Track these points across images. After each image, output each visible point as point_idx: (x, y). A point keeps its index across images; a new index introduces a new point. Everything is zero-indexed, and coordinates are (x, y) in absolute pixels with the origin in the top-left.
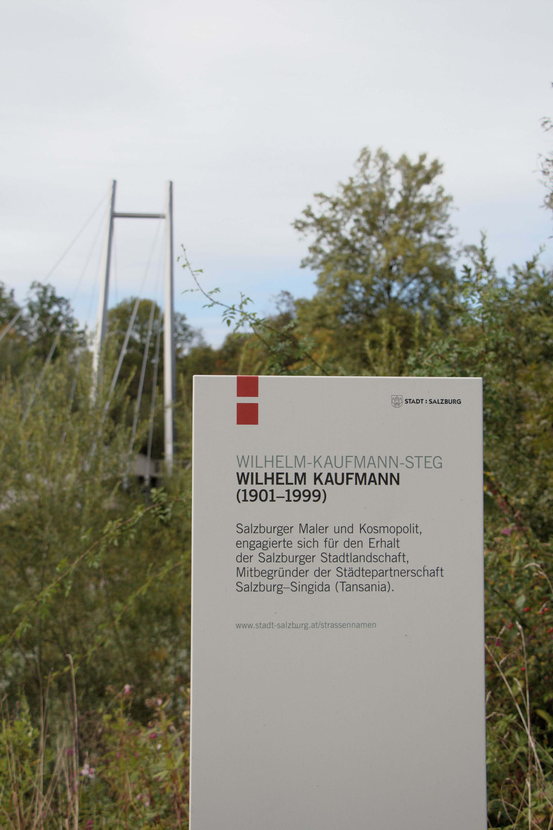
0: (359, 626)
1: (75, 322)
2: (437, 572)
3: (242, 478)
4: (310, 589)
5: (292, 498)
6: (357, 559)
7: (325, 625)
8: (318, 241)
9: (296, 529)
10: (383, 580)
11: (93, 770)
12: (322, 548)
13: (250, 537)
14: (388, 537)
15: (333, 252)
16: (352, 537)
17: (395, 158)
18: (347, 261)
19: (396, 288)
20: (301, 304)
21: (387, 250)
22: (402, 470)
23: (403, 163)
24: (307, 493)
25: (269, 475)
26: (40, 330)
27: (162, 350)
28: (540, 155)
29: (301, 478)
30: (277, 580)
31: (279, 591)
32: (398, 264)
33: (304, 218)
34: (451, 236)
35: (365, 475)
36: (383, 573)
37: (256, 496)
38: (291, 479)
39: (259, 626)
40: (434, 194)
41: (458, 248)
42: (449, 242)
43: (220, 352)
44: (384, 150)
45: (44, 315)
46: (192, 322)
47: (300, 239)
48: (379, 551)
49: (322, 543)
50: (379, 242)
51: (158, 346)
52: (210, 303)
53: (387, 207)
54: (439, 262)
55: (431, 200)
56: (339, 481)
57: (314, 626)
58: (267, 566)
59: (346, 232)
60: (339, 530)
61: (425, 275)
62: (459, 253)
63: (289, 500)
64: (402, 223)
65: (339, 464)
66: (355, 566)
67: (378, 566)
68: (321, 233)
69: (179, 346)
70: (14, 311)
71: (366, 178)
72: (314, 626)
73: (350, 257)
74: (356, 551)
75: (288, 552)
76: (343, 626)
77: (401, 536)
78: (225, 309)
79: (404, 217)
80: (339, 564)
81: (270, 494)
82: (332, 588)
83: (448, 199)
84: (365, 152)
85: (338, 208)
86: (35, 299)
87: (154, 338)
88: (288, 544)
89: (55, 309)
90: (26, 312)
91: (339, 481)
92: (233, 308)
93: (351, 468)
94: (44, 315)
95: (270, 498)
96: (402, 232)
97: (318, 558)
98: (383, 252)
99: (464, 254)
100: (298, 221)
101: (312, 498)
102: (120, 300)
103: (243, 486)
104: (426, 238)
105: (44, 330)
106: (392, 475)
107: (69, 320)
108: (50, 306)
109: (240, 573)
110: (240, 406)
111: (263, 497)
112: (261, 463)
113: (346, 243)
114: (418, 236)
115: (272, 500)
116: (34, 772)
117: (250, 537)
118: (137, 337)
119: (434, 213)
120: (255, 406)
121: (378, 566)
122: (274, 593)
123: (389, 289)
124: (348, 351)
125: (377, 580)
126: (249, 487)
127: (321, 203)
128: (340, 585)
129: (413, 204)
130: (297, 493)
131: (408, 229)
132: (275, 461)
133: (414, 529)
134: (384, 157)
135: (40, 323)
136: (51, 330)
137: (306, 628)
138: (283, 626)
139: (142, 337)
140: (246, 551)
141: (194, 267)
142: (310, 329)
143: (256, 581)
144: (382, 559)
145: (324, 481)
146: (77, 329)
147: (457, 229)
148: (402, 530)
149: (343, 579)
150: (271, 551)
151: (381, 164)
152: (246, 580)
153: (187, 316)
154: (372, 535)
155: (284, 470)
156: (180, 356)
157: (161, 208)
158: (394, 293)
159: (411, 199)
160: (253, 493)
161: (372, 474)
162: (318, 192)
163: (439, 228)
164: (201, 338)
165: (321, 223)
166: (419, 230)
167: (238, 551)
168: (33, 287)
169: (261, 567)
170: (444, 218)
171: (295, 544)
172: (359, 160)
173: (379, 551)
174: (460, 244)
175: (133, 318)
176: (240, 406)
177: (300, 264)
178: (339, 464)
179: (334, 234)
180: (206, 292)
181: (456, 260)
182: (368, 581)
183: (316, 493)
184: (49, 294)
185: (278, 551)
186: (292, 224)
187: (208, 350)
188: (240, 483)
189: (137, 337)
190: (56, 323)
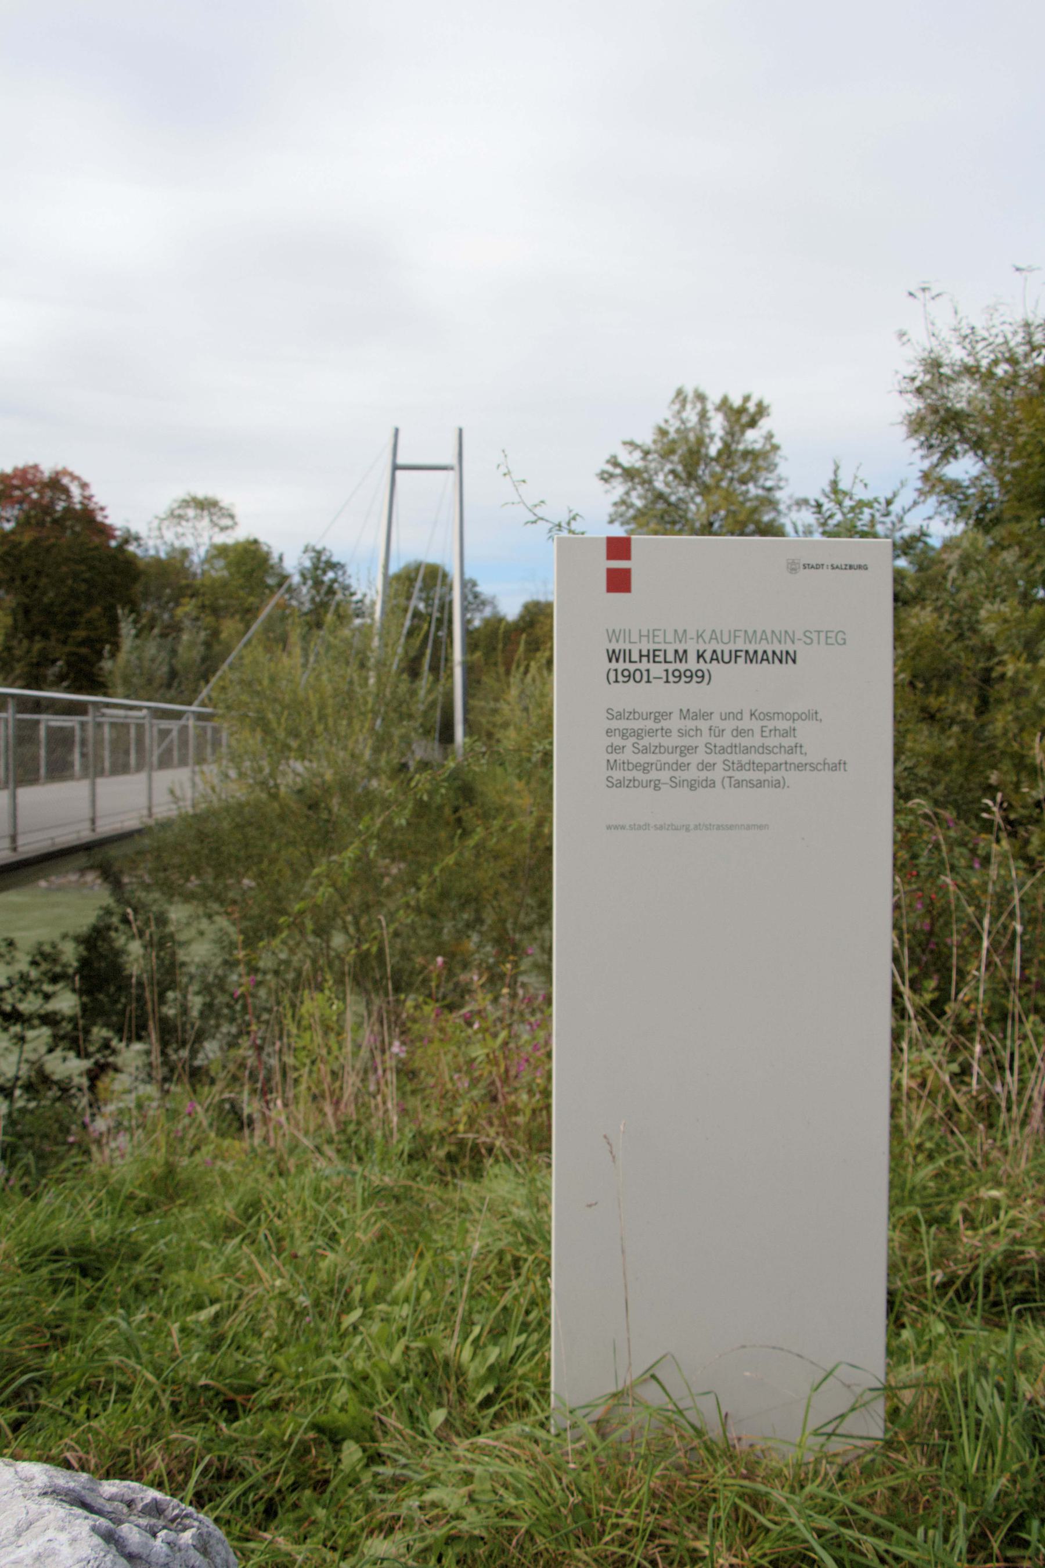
0: (749, 827)
1: (352, 590)
2: (835, 767)
3: (613, 656)
4: (692, 786)
5: (671, 678)
6: (747, 750)
7: (709, 827)
8: (627, 493)
9: (676, 715)
10: (777, 775)
11: (404, 1048)
12: (706, 738)
13: (622, 724)
14: (783, 725)
15: (646, 507)
17: (714, 398)
18: (662, 517)
21: (708, 505)
22: (799, 648)
23: (724, 405)
24: (688, 674)
25: (644, 653)
26: (313, 600)
27: (450, 621)
28: (897, 372)
29: (681, 656)
30: (654, 775)
31: (657, 787)
33: (610, 468)
34: (780, 488)
35: (756, 652)
36: (777, 767)
37: (630, 676)
38: (670, 657)
39: (633, 827)
40: (761, 441)
41: (789, 502)
42: (778, 495)
44: (701, 389)
45: (318, 583)
46: (484, 588)
47: (607, 492)
48: (773, 741)
49: (706, 732)
50: (698, 494)
51: (446, 616)
52: (534, 518)
53: (707, 455)
54: (766, 518)
55: (758, 446)
56: (726, 659)
57: (697, 827)
58: (643, 758)
59: (659, 484)
60: (725, 717)
62: (789, 508)
63: (667, 682)
64: (723, 473)
65: (726, 639)
66: (745, 758)
67: (771, 759)
68: (630, 484)
69: (469, 616)
70: (284, 578)
71: (683, 422)
72: (697, 827)
73: (665, 512)
74: (746, 741)
75: (666, 742)
76: (731, 827)
77: (798, 724)
78: (550, 525)
79: (726, 467)
81: (645, 674)
82: (718, 784)
84: (679, 392)
85: (650, 457)
86: (308, 564)
87: (442, 608)
88: (667, 733)
89: (331, 575)
90: (296, 579)
91: (726, 659)
92: (559, 525)
93: (740, 645)
94: (318, 583)
95: (645, 678)
97: (702, 749)
98: (703, 508)
99: (795, 508)
100: (603, 472)
101: (695, 679)
102: (402, 564)
103: (614, 665)
104: (753, 490)
105: (318, 599)
106: (787, 653)
107: (346, 588)
108: (325, 573)
109: (611, 765)
111: (638, 678)
112: (635, 638)
113: (660, 496)
114: (744, 488)
115: (648, 681)
116: (340, 1048)
117: (622, 724)
118: (421, 606)
119: (761, 463)
121: (771, 759)
122: (650, 790)
125: (770, 775)
126: (621, 666)
127: (630, 453)
128: (727, 781)
129: (736, 451)
130: (677, 674)
131: (732, 479)
132: (651, 635)
133: (812, 715)
134: (701, 397)
135: (314, 592)
136: (326, 599)
137: (688, 830)
138: (661, 828)
139: (427, 606)
140: (617, 741)
141: (517, 476)
143: (629, 775)
144: (776, 750)
145: (708, 659)
146: (355, 598)
147: (787, 480)
148: (800, 717)
149: (730, 773)
150: (646, 741)
151: (699, 406)
152: (617, 775)
153: (479, 582)
154: (765, 723)
155: (662, 647)
156: (471, 627)
157: (449, 457)
159: (734, 447)
160: (626, 673)
161: (765, 652)
162: (628, 439)
163: (766, 479)
164: (495, 607)
165: (630, 474)
166: (743, 481)
167: (609, 741)
168: (306, 551)
170: (772, 467)
171: (675, 733)
172: (673, 402)
173: (773, 741)
174: (790, 497)
175: (418, 584)
177: (607, 519)
178: (726, 639)
179: (646, 486)
180: (529, 505)
181: (786, 515)
182: (759, 775)
183: (700, 674)
184: (324, 558)
185: (655, 741)
187: (500, 620)
188: (610, 660)
189: (421, 606)
190: (331, 591)
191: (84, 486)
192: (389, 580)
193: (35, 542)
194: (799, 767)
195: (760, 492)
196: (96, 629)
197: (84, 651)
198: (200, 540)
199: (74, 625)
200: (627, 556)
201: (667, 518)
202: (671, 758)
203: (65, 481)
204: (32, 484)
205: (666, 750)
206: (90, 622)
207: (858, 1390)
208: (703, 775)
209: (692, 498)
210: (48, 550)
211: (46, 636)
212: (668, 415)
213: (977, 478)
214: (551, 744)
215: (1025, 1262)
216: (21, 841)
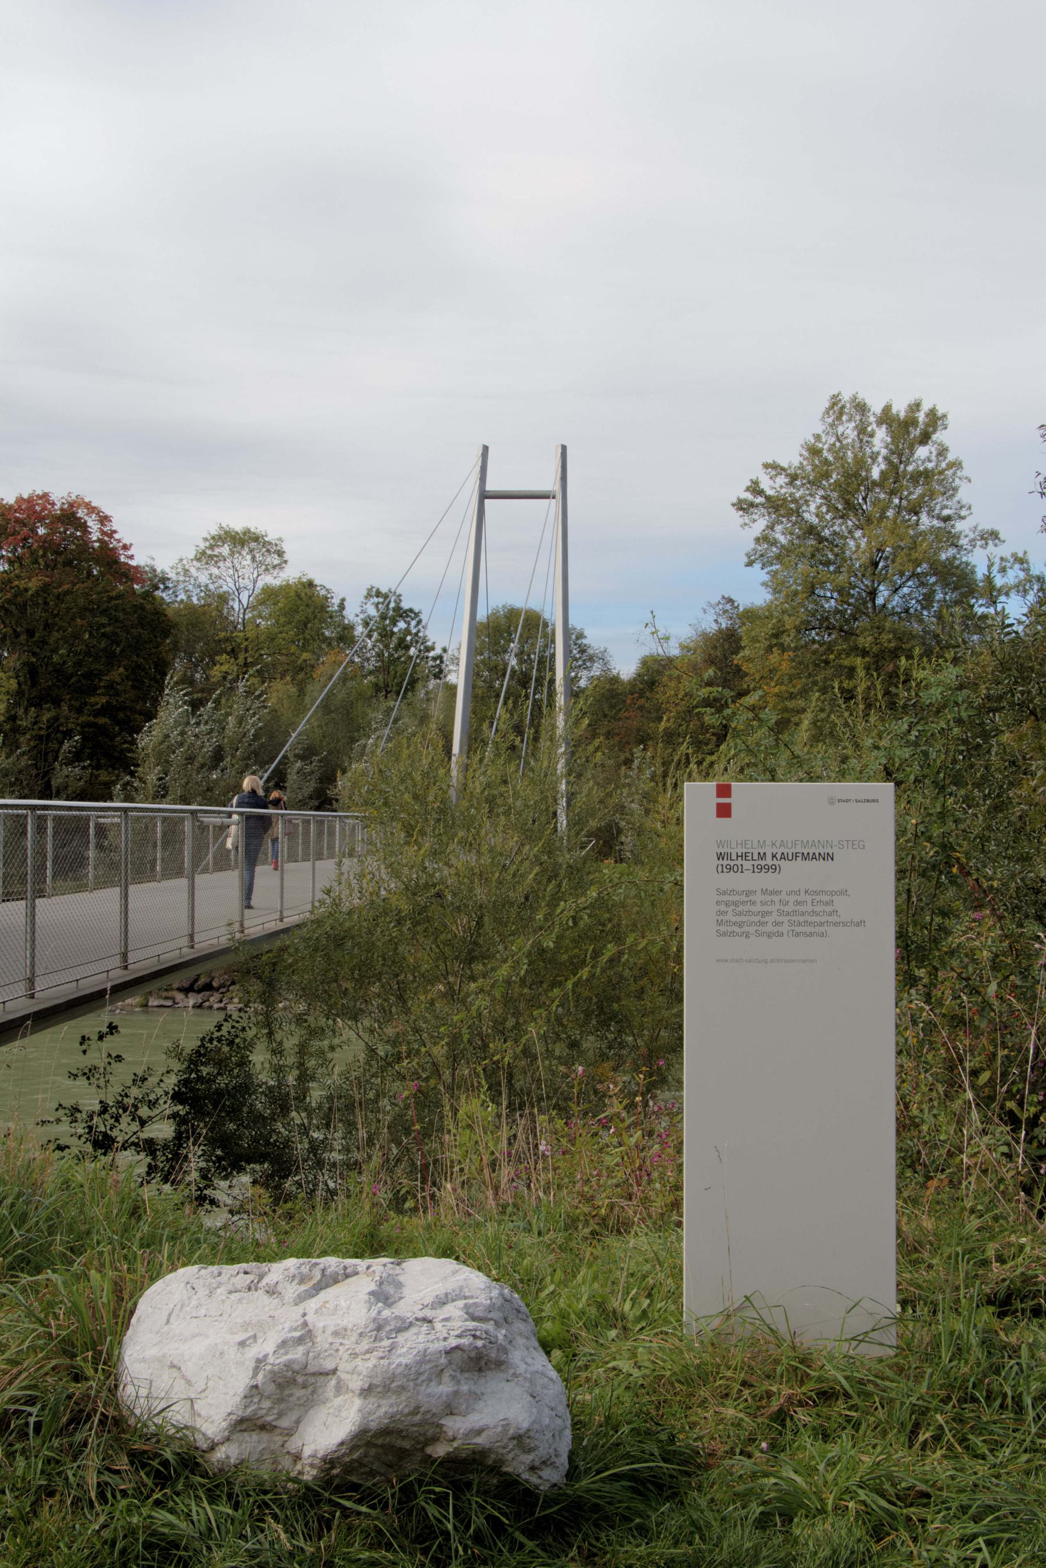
0: (804, 961)
2: (859, 924)
3: (720, 856)
4: (769, 935)
6: (803, 914)
7: (779, 961)
8: (771, 527)
9: (759, 892)
10: (821, 929)
12: (777, 906)
13: (726, 898)
14: (826, 898)
16: (799, 898)
17: (876, 407)
19: (883, 593)
20: (750, 615)
22: (835, 851)
23: (887, 418)
26: (380, 655)
29: (762, 856)
30: (745, 929)
31: (747, 937)
32: (887, 558)
33: (749, 496)
36: (821, 924)
37: (730, 869)
38: (756, 857)
42: (960, 526)
43: (633, 683)
45: (386, 635)
46: (594, 639)
48: (819, 908)
49: (777, 903)
50: (858, 527)
55: (930, 466)
57: (772, 961)
61: (926, 574)
65: (790, 846)
66: (801, 919)
72: (772, 961)
74: (803, 908)
75: (753, 909)
77: (835, 898)
79: (892, 493)
80: (790, 917)
82: (785, 934)
83: (956, 465)
84: (835, 400)
87: (541, 662)
88: (753, 903)
89: (402, 625)
93: (799, 849)
96: (890, 513)
97: (775, 914)
98: (863, 543)
103: (721, 862)
107: (417, 639)
108: (394, 623)
109: (719, 923)
110: (719, 805)
112: (734, 845)
117: (726, 898)
120: (718, 796)
122: (743, 938)
123: (873, 594)
124: (815, 683)
125: (819, 929)
126: (725, 862)
133: (844, 892)
134: (862, 408)
140: (723, 908)
142: (762, 652)
143: (730, 929)
149: (793, 928)
150: (741, 908)
152: (723, 929)
155: (751, 851)
157: (549, 483)
158: (880, 601)
162: (770, 461)
168: (368, 596)
169: (734, 919)
171: (758, 903)
173: (819, 908)
176: (719, 805)
178: (790, 846)
182: (809, 929)
185: (746, 908)
186: (733, 505)
187: (615, 680)
191: (104, 519)
192: (475, 629)
193: (45, 588)
194: (835, 924)
195: (936, 523)
196: (117, 694)
197: (102, 720)
198: (242, 583)
199: (93, 690)
200: (729, 795)
201: (818, 556)
202: (756, 919)
203: (81, 513)
204: (41, 519)
205: (753, 913)
206: (111, 686)
207: (878, 1317)
208: (776, 929)
209: (850, 532)
210: (59, 598)
211: (57, 702)
212: (819, 429)
213: (197, 1448)
214: (682, 875)
215: (1036, 1284)
216: (132, 957)
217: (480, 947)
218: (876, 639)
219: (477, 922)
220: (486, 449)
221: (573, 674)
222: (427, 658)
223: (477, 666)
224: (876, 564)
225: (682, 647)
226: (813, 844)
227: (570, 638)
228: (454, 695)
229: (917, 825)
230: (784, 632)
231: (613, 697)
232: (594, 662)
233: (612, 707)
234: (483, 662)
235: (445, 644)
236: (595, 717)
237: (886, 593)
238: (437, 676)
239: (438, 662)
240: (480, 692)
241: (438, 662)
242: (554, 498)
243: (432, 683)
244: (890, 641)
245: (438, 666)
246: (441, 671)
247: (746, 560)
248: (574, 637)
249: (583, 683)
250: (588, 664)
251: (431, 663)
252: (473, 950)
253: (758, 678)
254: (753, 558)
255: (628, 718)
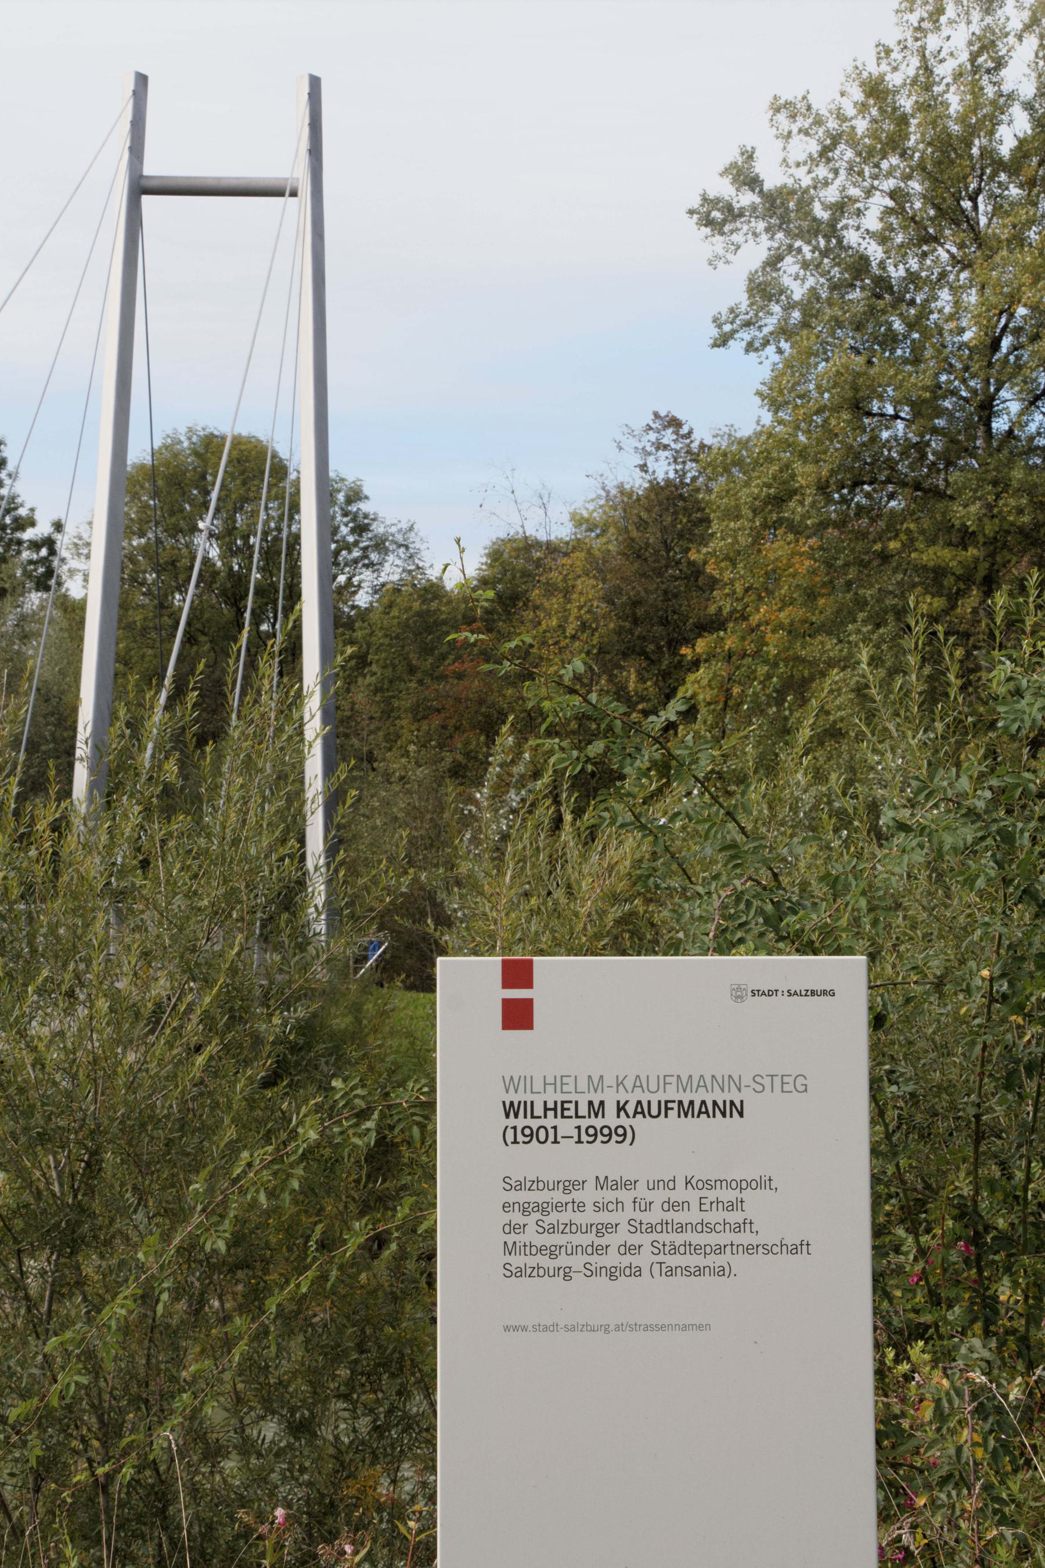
0: (685, 1328)
3: (510, 1110)
4: (612, 1274)
6: (682, 1228)
7: (634, 1327)
8: (774, 262)
9: (591, 1183)
10: (721, 1260)
12: (629, 1213)
13: (523, 1196)
14: (728, 1195)
22: (747, 1096)
29: (597, 1109)
30: (563, 1261)
31: (567, 1277)
32: (1018, 331)
36: (720, 1249)
37: (532, 1135)
38: (583, 1110)
48: (713, 1217)
65: (653, 1087)
66: (679, 1239)
72: (618, 1328)
75: (579, 1218)
77: (747, 1195)
80: (654, 1236)
82: (645, 1272)
87: (270, 555)
88: (580, 1206)
97: (624, 1227)
103: (512, 1121)
109: (509, 1249)
112: (538, 1086)
117: (523, 1196)
123: (987, 408)
124: (861, 603)
126: (521, 1122)
133: (765, 1183)
140: (517, 1218)
143: (532, 1261)
149: (661, 1258)
150: (553, 1217)
152: (517, 1261)
155: (573, 1097)
158: (1000, 425)
169: (539, 1240)
171: (590, 1207)
178: (653, 1087)
185: (565, 1217)
187: (433, 591)
194: (749, 1249)
202: (585, 1239)
208: (626, 1260)
217: (93, 1215)
218: (990, 507)
219: (88, 1164)
220: (142, 80)
221: (342, 579)
222: (20, 542)
223: (132, 559)
224: (995, 345)
225: (578, 521)
226: (702, 1084)
227: (333, 502)
228: (81, 623)
229: (992, 980)
230: (795, 492)
231: (429, 629)
232: (387, 551)
233: (426, 650)
234: (144, 550)
235: (58, 514)
236: (389, 672)
237: (1015, 407)
238: (42, 585)
239: (44, 552)
240: (138, 617)
241: (44, 552)
242: (294, 194)
243: (35, 598)
244: (1020, 511)
245: (45, 561)
246: (50, 573)
247: (714, 332)
248: (341, 497)
249: (362, 599)
250: (374, 556)
251: (26, 555)
252: (79, 1223)
253: (739, 588)
254: (727, 328)
255: (460, 676)
